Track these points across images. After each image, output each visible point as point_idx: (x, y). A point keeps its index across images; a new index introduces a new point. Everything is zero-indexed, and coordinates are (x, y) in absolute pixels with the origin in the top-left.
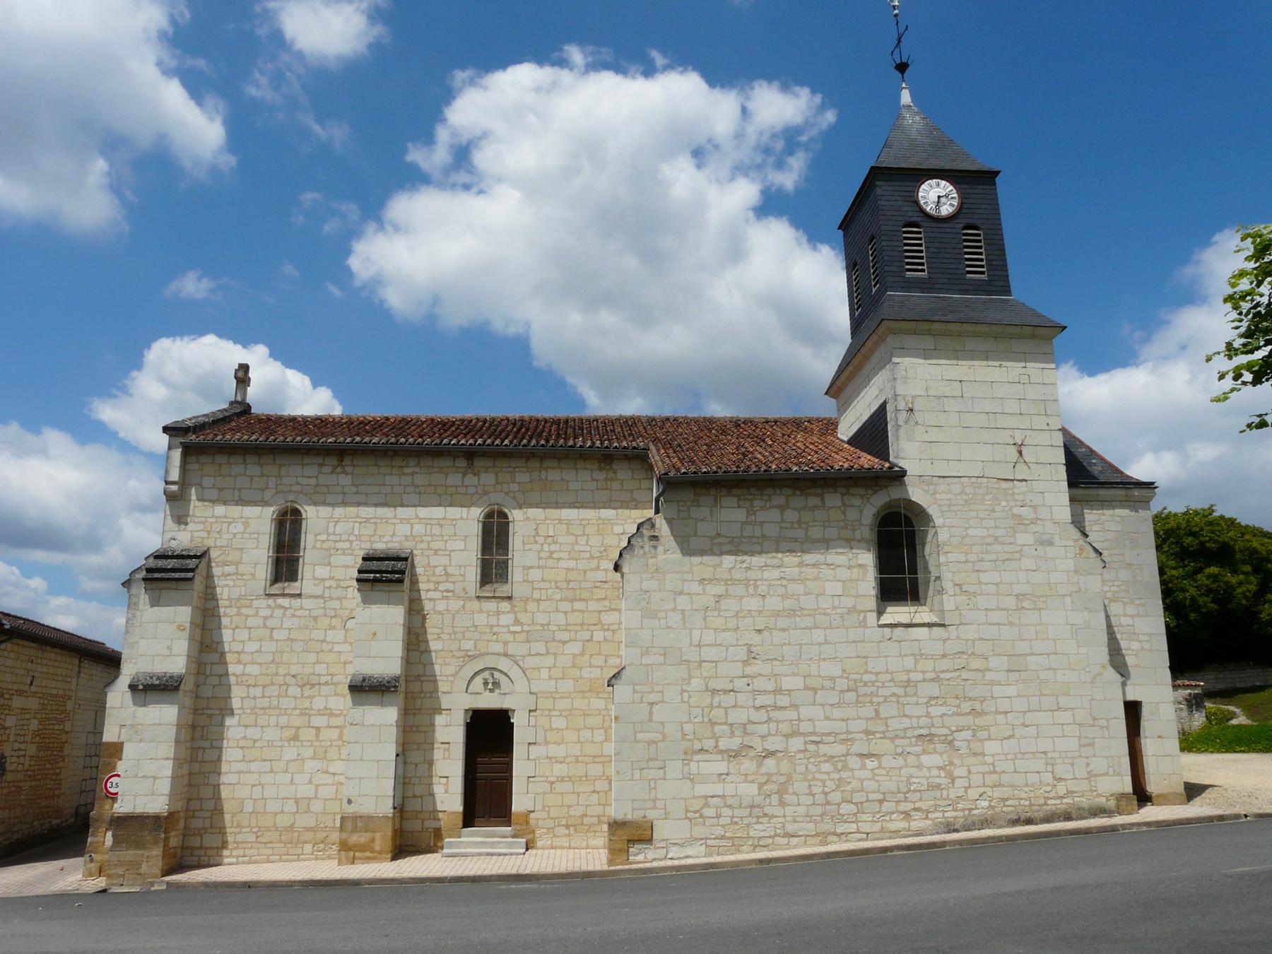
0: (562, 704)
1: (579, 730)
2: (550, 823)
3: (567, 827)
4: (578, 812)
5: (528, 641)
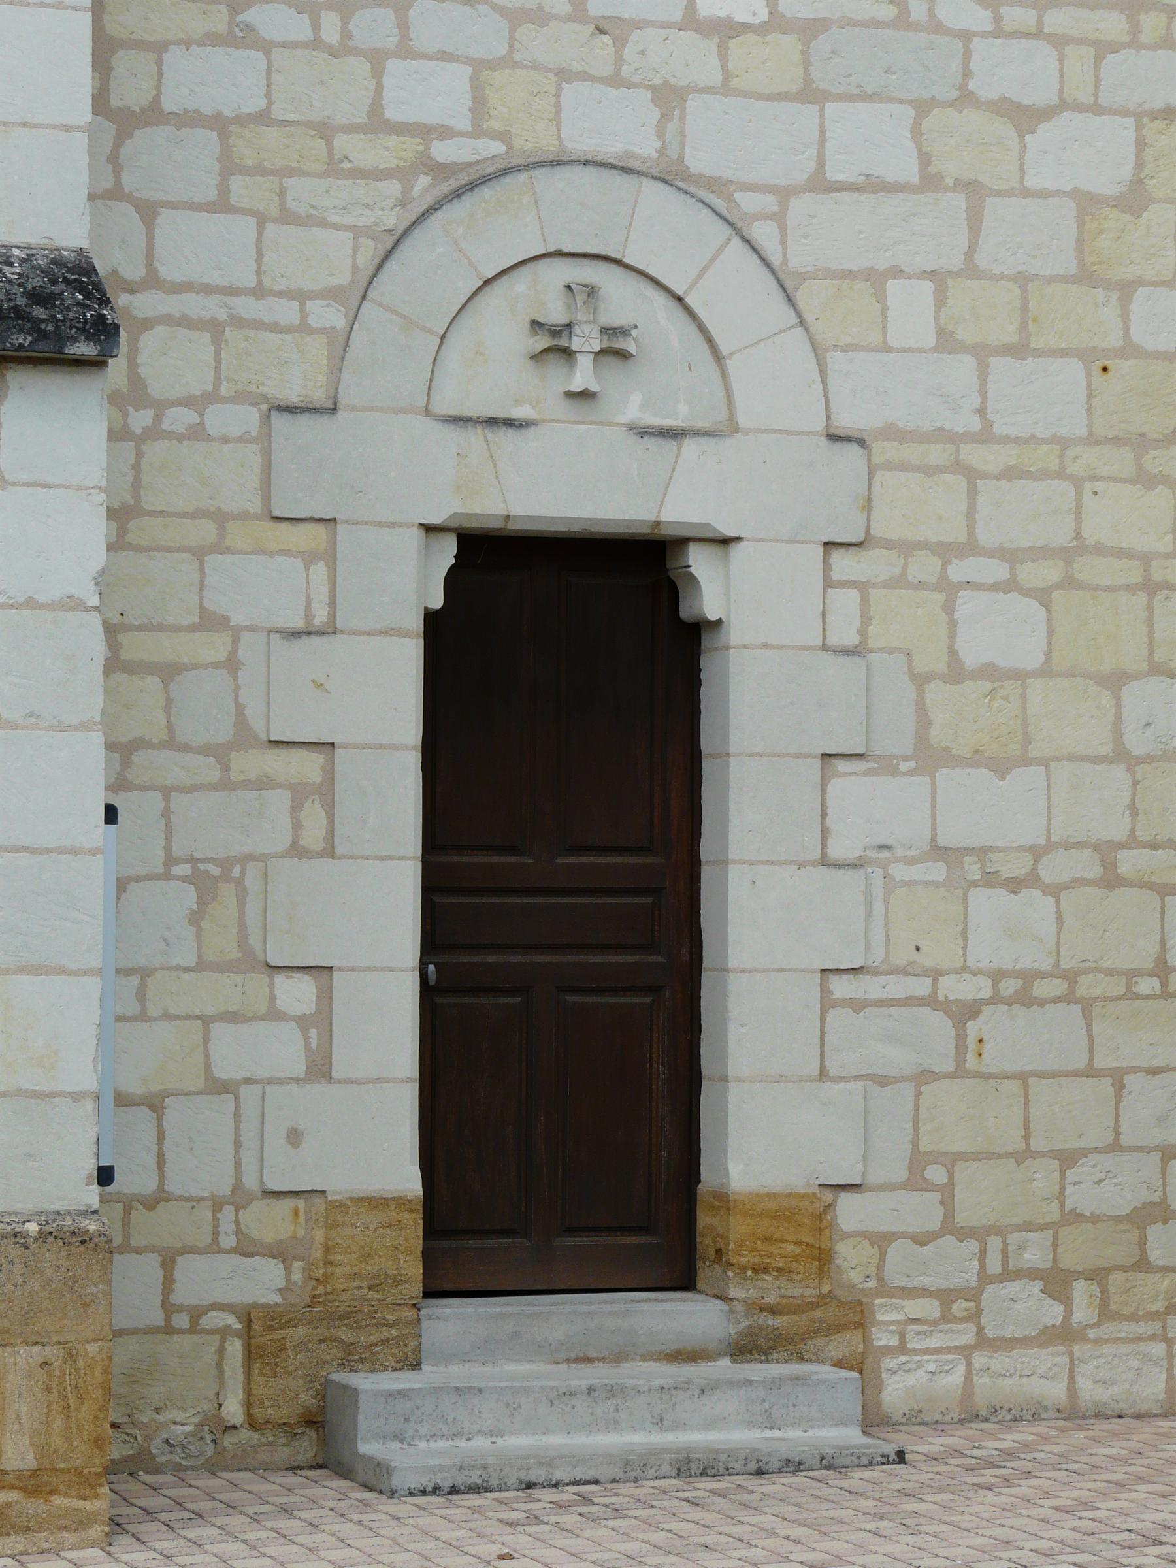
0: (1021, 514)
1: (1115, 681)
2: (955, 1263)
3: (1056, 1282)
4: (1108, 1188)
5: (810, 93)
